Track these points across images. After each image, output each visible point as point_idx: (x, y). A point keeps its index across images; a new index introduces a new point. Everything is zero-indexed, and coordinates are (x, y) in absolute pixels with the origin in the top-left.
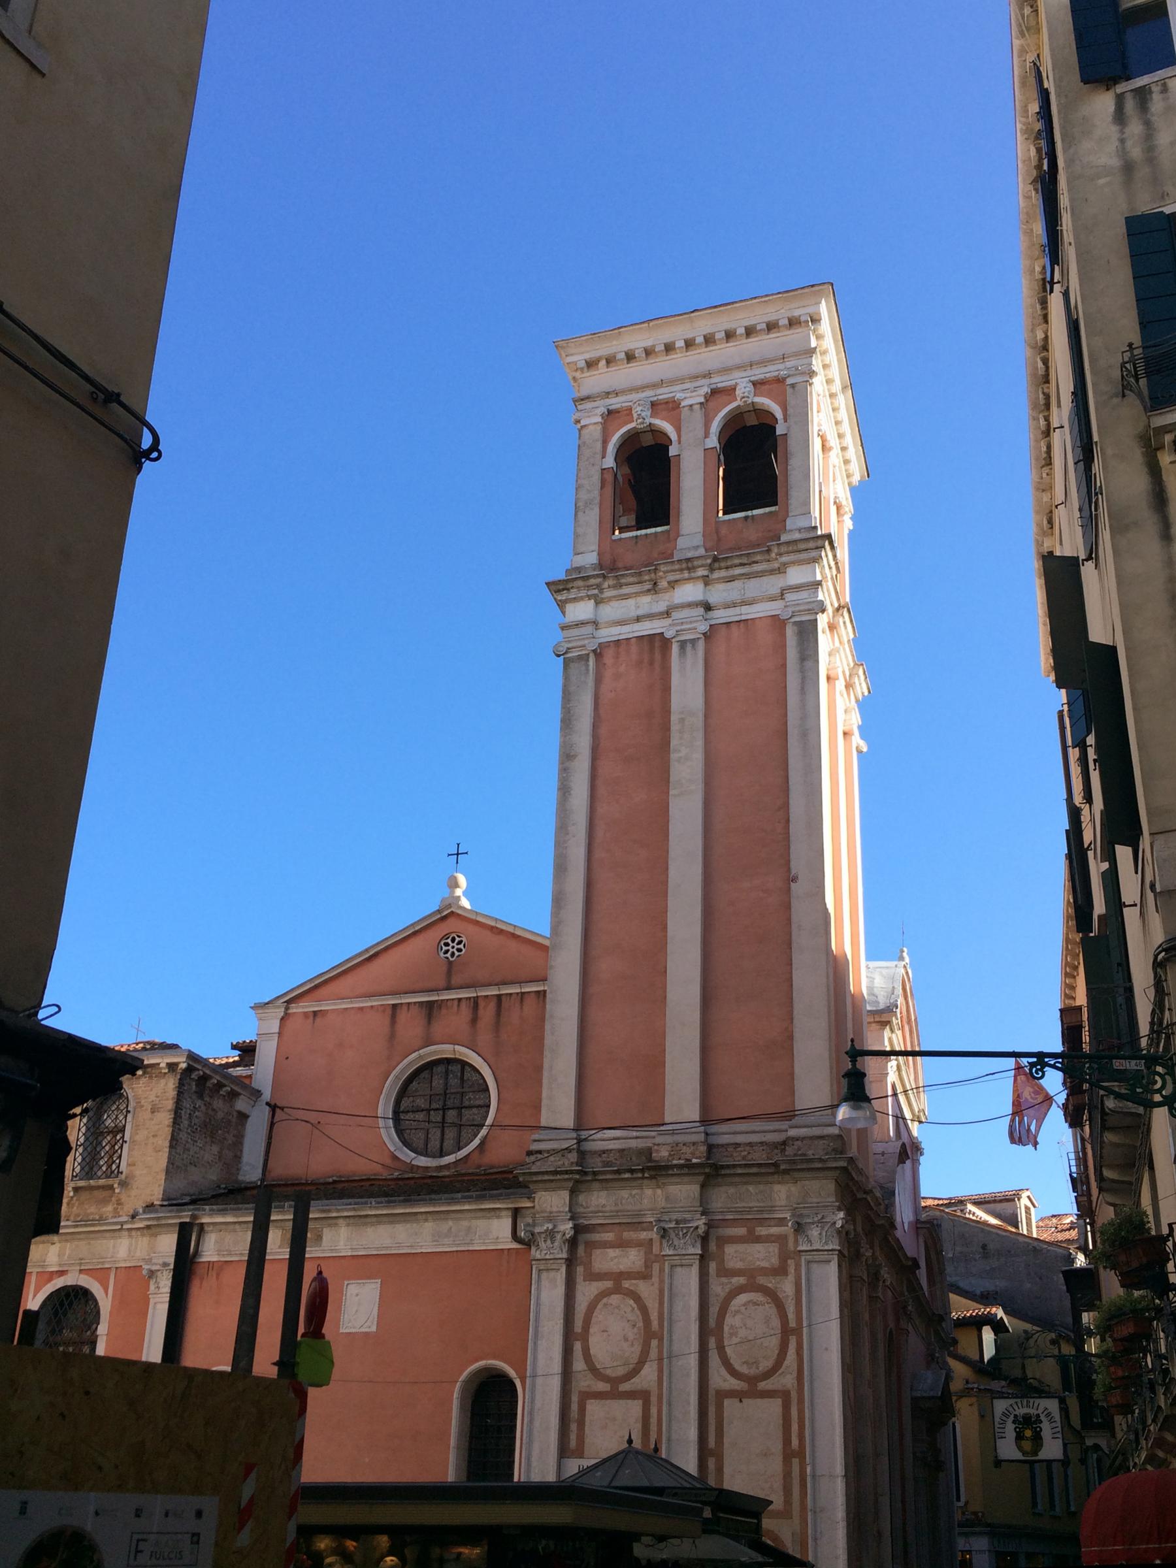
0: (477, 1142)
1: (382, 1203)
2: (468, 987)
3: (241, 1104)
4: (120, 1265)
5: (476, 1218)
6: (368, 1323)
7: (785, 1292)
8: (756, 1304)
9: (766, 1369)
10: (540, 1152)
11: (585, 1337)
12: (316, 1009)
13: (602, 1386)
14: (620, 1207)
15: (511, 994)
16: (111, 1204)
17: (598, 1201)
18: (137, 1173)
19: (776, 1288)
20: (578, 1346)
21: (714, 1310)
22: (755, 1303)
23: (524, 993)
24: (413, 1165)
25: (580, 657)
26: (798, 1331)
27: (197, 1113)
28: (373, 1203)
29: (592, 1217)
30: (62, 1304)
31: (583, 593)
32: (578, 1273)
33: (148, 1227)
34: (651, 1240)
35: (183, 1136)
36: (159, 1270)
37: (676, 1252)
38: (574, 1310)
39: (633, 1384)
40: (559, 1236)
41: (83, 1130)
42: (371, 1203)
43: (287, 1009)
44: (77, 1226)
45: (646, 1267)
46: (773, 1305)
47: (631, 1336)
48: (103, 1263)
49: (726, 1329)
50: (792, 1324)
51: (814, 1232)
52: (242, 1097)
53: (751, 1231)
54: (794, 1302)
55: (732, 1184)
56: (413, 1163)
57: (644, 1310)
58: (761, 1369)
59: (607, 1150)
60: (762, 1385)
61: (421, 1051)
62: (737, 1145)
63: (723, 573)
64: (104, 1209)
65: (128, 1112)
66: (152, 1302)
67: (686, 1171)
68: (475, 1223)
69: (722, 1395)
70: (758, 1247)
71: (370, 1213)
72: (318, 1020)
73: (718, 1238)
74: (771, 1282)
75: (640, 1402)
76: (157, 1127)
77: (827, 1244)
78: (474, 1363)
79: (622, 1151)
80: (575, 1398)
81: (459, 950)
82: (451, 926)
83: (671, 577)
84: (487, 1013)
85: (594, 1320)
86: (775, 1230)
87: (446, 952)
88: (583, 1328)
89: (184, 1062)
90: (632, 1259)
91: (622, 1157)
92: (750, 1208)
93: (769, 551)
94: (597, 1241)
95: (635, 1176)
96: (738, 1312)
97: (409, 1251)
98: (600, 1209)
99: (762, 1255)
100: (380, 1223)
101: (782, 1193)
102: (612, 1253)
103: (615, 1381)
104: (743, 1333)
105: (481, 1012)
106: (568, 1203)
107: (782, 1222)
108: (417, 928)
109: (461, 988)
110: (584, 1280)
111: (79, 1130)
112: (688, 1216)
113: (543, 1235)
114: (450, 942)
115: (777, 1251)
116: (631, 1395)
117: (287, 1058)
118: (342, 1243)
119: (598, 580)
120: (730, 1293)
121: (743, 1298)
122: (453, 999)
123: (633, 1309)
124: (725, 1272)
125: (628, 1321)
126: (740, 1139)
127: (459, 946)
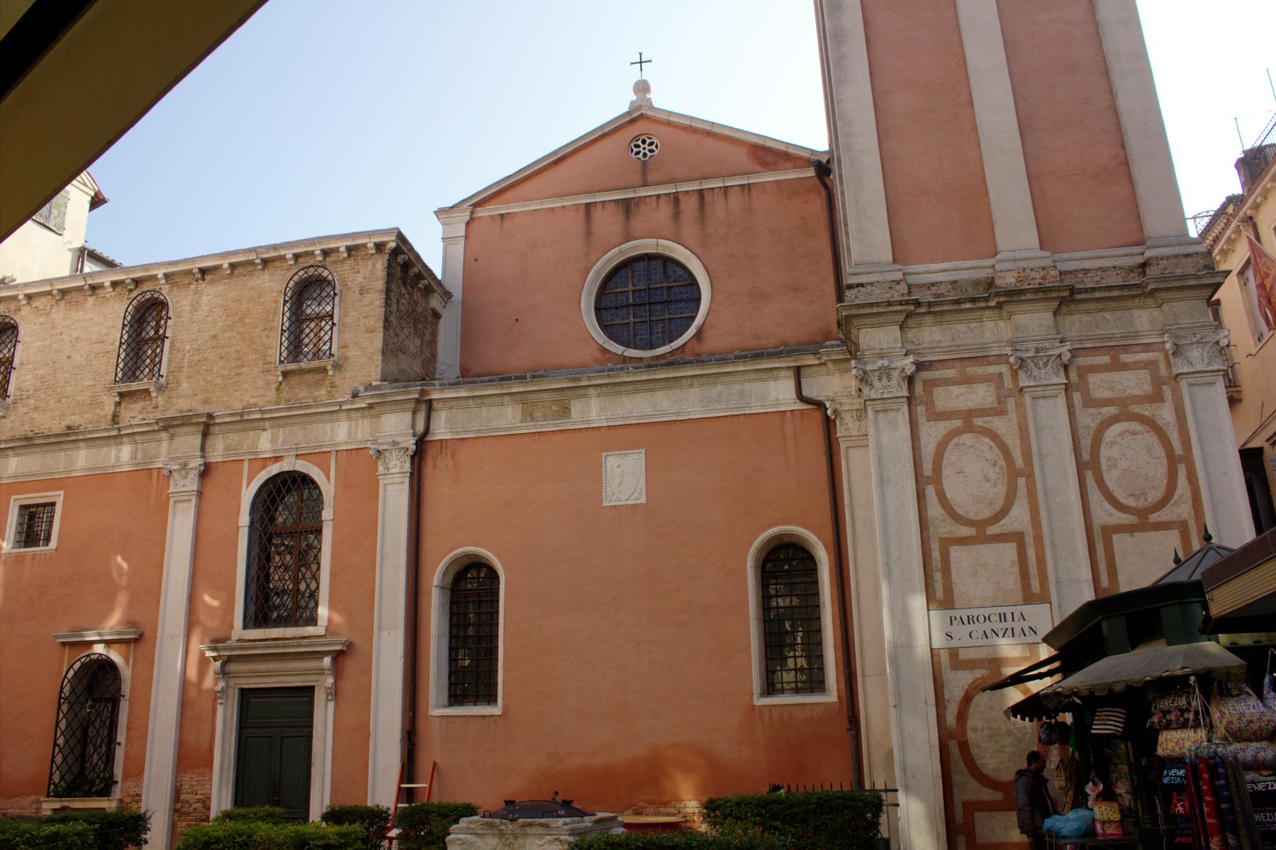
0: (692, 331)
1: (641, 368)
2: (666, 183)
3: (435, 302)
4: (341, 448)
5: (750, 381)
6: (636, 495)
7: (1164, 419)
8: (1133, 433)
9: (1156, 500)
10: (862, 285)
12: (502, 212)
13: (965, 531)
14: (959, 342)
15: (713, 189)
16: (324, 388)
17: (932, 336)
18: (350, 354)
19: (1154, 415)
20: (930, 491)
21: (1086, 443)
22: (1132, 432)
23: (727, 187)
27: (402, 300)
29: (926, 353)
30: (279, 491)
32: (919, 413)
33: (371, 406)
34: (1001, 374)
35: (393, 319)
36: (386, 450)
37: (1037, 383)
38: (920, 452)
39: (1001, 526)
40: (895, 374)
41: (288, 314)
42: (628, 369)
43: (472, 213)
44: (290, 409)
45: (1000, 402)
47: (992, 476)
48: (321, 446)
49: (1103, 461)
50: (1178, 451)
51: (1195, 353)
52: (436, 294)
53: (1115, 359)
54: (1176, 429)
55: (1089, 312)
56: (625, 354)
58: (1150, 500)
59: (937, 283)
60: (1154, 518)
61: (622, 246)
62: (1086, 271)
64: (317, 393)
65: (335, 294)
66: (381, 484)
67: (1041, 295)
68: (748, 386)
69: (1108, 531)
70: (1126, 374)
71: (627, 379)
72: (506, 222)
73: (1079, 368)
74: (1147, 410)
75: (1014, 544)
76: (367, 308)
77: (1210, 365)
78: (766, 530)
79: (954, 283)
80: (935, 546)
81: (651, 151)
84: (689, 207)
85: (945, 462)
86: (1142, 356)
87: (638, 153)
88: (933, 470)
89: (393, 241)
90: (981, 395)
91: (954, 289)
92: (1112, 334)
95: (978, 305)
96: (1113, 443)
97: (675, 418)
98: (936, 345)
99: (1133, 383)
100: (637, 391)
101: (1143, 319)
102: (955, 390)
103: (981, 525)
104: (1123, 464)
105: (683, 207)
107: (1148, 347)
108: (606, 130)
109: (659, 184)
110: (928, 421)
111: (283, 314)
112: (1046, 345)
113: (877, 373)
114: (641, 144)
115: (1148, 377)
116: (1002, 538)
117: (476, 260)
118: (594, 414)
120: (1102, 423)
121: (1116, 429)
122: (651, 196)
123: (991, 447)
124: (1090, 402)
127: (651, 147)
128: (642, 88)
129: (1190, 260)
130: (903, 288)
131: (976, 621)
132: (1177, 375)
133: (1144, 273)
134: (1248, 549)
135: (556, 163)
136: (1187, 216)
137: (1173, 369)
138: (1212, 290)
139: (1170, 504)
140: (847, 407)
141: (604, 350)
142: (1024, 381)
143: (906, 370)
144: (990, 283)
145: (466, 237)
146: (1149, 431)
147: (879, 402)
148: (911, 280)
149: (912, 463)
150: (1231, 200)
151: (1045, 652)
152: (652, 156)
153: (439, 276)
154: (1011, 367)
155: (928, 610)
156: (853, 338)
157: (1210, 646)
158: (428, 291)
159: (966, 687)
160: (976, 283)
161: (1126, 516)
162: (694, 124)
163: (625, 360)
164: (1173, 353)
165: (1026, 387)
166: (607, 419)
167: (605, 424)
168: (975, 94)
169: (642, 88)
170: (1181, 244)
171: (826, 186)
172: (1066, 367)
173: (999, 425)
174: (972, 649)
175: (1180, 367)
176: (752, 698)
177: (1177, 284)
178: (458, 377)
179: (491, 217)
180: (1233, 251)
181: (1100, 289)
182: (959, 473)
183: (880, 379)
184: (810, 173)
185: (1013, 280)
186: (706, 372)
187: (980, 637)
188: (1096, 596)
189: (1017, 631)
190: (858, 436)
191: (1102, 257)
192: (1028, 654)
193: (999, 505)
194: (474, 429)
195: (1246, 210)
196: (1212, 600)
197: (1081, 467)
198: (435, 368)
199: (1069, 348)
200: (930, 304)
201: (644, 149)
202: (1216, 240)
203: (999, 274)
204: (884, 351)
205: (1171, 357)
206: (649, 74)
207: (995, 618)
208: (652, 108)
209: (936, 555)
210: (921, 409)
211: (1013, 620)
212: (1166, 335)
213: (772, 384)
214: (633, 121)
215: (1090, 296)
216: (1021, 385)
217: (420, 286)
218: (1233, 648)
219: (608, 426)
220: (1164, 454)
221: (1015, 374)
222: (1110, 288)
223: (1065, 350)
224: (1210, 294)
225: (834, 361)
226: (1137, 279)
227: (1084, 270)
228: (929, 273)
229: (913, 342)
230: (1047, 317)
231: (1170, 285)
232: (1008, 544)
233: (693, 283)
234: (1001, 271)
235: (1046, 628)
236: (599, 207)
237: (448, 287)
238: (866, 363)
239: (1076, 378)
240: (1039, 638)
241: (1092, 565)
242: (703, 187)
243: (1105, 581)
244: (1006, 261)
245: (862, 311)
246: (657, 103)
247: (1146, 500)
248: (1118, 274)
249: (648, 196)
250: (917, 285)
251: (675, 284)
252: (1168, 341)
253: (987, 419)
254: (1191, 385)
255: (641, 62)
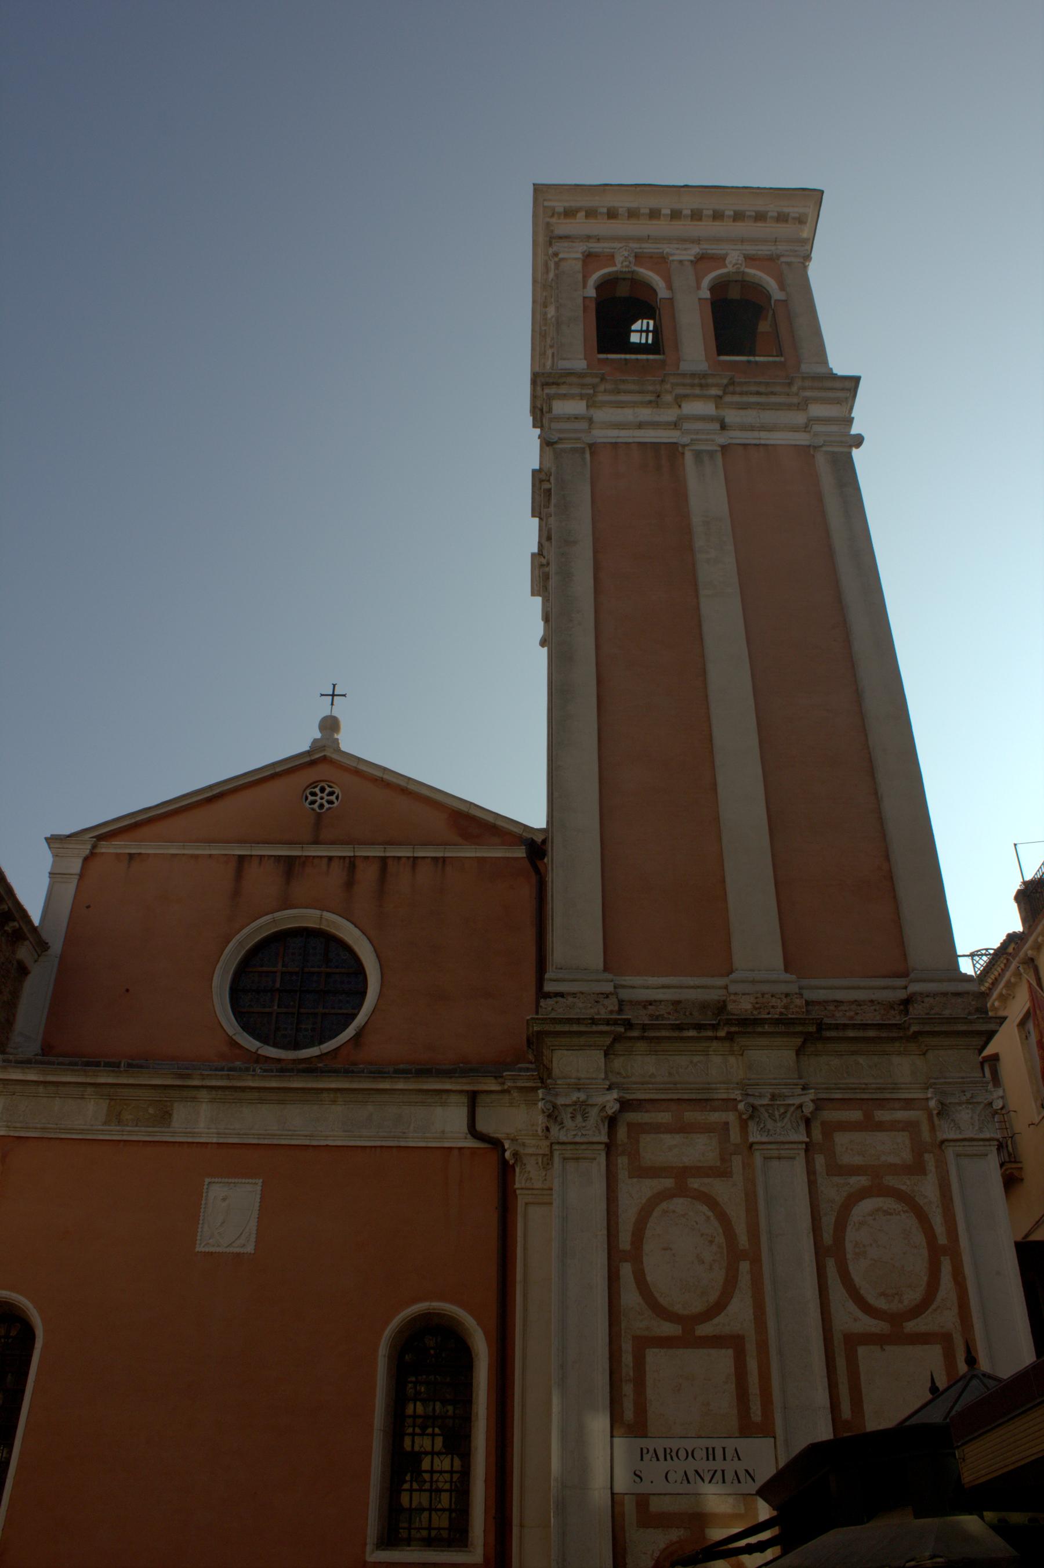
3: (24, 952)
8: (887, 1213)
10: (561, 995)
11: (636, 1255)
13: (669, 1329)
15: (399, 858)
20: (626, 1270)
21: (828, 1221)
24: (259, 1055)
25: (574, 450)
26: (954, 1251)
28: (258, 1071)
31: (576, 391)
32: (620, 1166)
34: (727, 1123)
37: (771, 1139)
38: (617, 1217)
40: (594, 1112)
42: (254, 1070)
43: (94, 847)
45: (723, 1160)
46: (912, 1214)
49: (849, 1246)
50: (942, 1240)
51: (964, 1115)
52: (27, 943)
57: (723, 1219)
58: (906, 1302)
59: (655, 1001)
60: (910, 1326)
61: (278, 915)
62: (838, 1003)
63: (736, 398)
67: (782, 1028)
69: (853, 1341)
73: (823, 1123)
75: (730, 1352)
79: (677, 1003)
80: (627, 1346)
81: (330, 802)
82: (322, 772)
83: (681, 391)
84: (368, 875)
86: (900, 1115)
87: (313, 802)
88: (633, 1243)
91: (676, 1011)
92: (866, 1084)
93: (790, 384)
94: (646, 1124)
95: (704, 1034)
97: (307, 1143)
102: (668, 1139)
103: (688, 1322)
106: (603, 1067)
107: (908, 1104)
108: (278, 770)
109: (333, 843)
112: (786, 1091)
113: (570, 1110)
114: (314, 798)
117: (88, 907)
119: (597, 380)
121: (867, 1205)
122: (321, 857)
124: (836, 1169)
125: (702, 1235)
126: (839, 995)
128: (330, 725)
129: (960, 1000)
130: (612, 1004)
131: (675, 1458)
132: (943, 1142)
133: (906, 1012)
134: (1023, 1378)
135: (210, 800)
136: (959, 953)
137: (938, 1133)
138: (984, 1039)
139: (930, 1310)
140: (530, 1151)
141: (233, 1044)
142: (755, 1136)
143: (607, 1108)
144: (721, 1007)
145: (81, 876)
146: (906, 1212)
147: (569, 1147)
148: (624, 994)
149: (605, 1232)
150: (1011, 938)
151: (764, 1511)
152: (330, 808)
153: (36, 921)
154: (740, 1115)
155: (612, 1436)
156: (546, 1062)
157: (971, 1523)
158: (18, 936)
159: (656, 1554)
160: (704, 1006)
161: (876, 1322)
162: (386, 777)
163: (258, 1058)
164: (938, 1114)
165: (757, 1143)
166: (218, 1134)
167: (215, 1140)
168: (720, 779)
169: (330, 725)
170: (950, 980)
171: (537, 871)
172: (808, 1122)
173: (720, 1189)
174: (667, 1496)
175: (947, 1132)
176: (364, 1552)
177: (945, 1028)
178: (37, 1055)
179: (118, 855)
180: (1014, 997)
181: (854, 1027)
182: (665, 1249)
183: (573, 1118)
184: (520, 852)
185: (749, 1007)
186: (355, 1086)
187: (679, 1481)
188: (834, 1435)
189: (730, 1475)
190: (543, 1189)
191: (859, 988)
192: (743, 1511)
193: (713, 1297)
194: (39, 1126)
195: (1027, 950)
196: (964, 1460)
197: (820, 1253)
198: (8, 1038)
199: (812, 1097)
200: (644, 1027)
201: (322, 798)
202: (995, 983)
203: (732, 997)
204: (582, 1082)
205: (936, 1119)
206: (340, 710)
207: (700, 1454)
208: (338, 750)
209: (627, 1359)
210: (622, 1161)
211: (725, 1459)
212: (931, 1090)
213: (439, 1110)
214: (313, 763)
215: (841, 1034)
216: (751, 1140)
217: (6, 928)
218: (1000, 1528)
219: (218, 1143)
220: (925, 1244)
221: (744, 1125)
222: (865, 1026)
223: (807, 1099)
224: (982, 1043)
225: (521, 1089)
226: (898, 1018)
227: (835, 1001)
228: (648, 988)
229: (619, 1073)
230: (788, 1056)
231: (936, 1029)
232: (724, 1351)
233: (360, 972)
234: (736, 994)
235: (766, 1472)
236: (266, 858)
237: (45, 936)
238: (556, 1095)
239: (820, 1136)
240: (753, 1488)
241: (830, 1386)
242: (388, 854)
243: (846, 1412)
244: (743, 982)
245: (559, 1028)
246: (344, 747)
247: (901, 1301)
248: (875, 1010)
249: (318, 857)
250: (631, 1002)
251: (338, 970)
252: (932, 1098)
253: (706, 1180)
254: (958, 1155)
255: (333, 695)
